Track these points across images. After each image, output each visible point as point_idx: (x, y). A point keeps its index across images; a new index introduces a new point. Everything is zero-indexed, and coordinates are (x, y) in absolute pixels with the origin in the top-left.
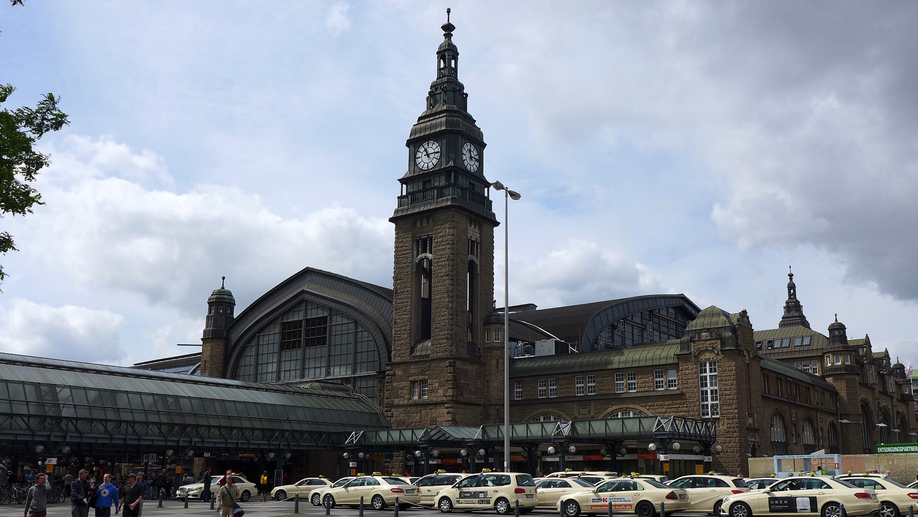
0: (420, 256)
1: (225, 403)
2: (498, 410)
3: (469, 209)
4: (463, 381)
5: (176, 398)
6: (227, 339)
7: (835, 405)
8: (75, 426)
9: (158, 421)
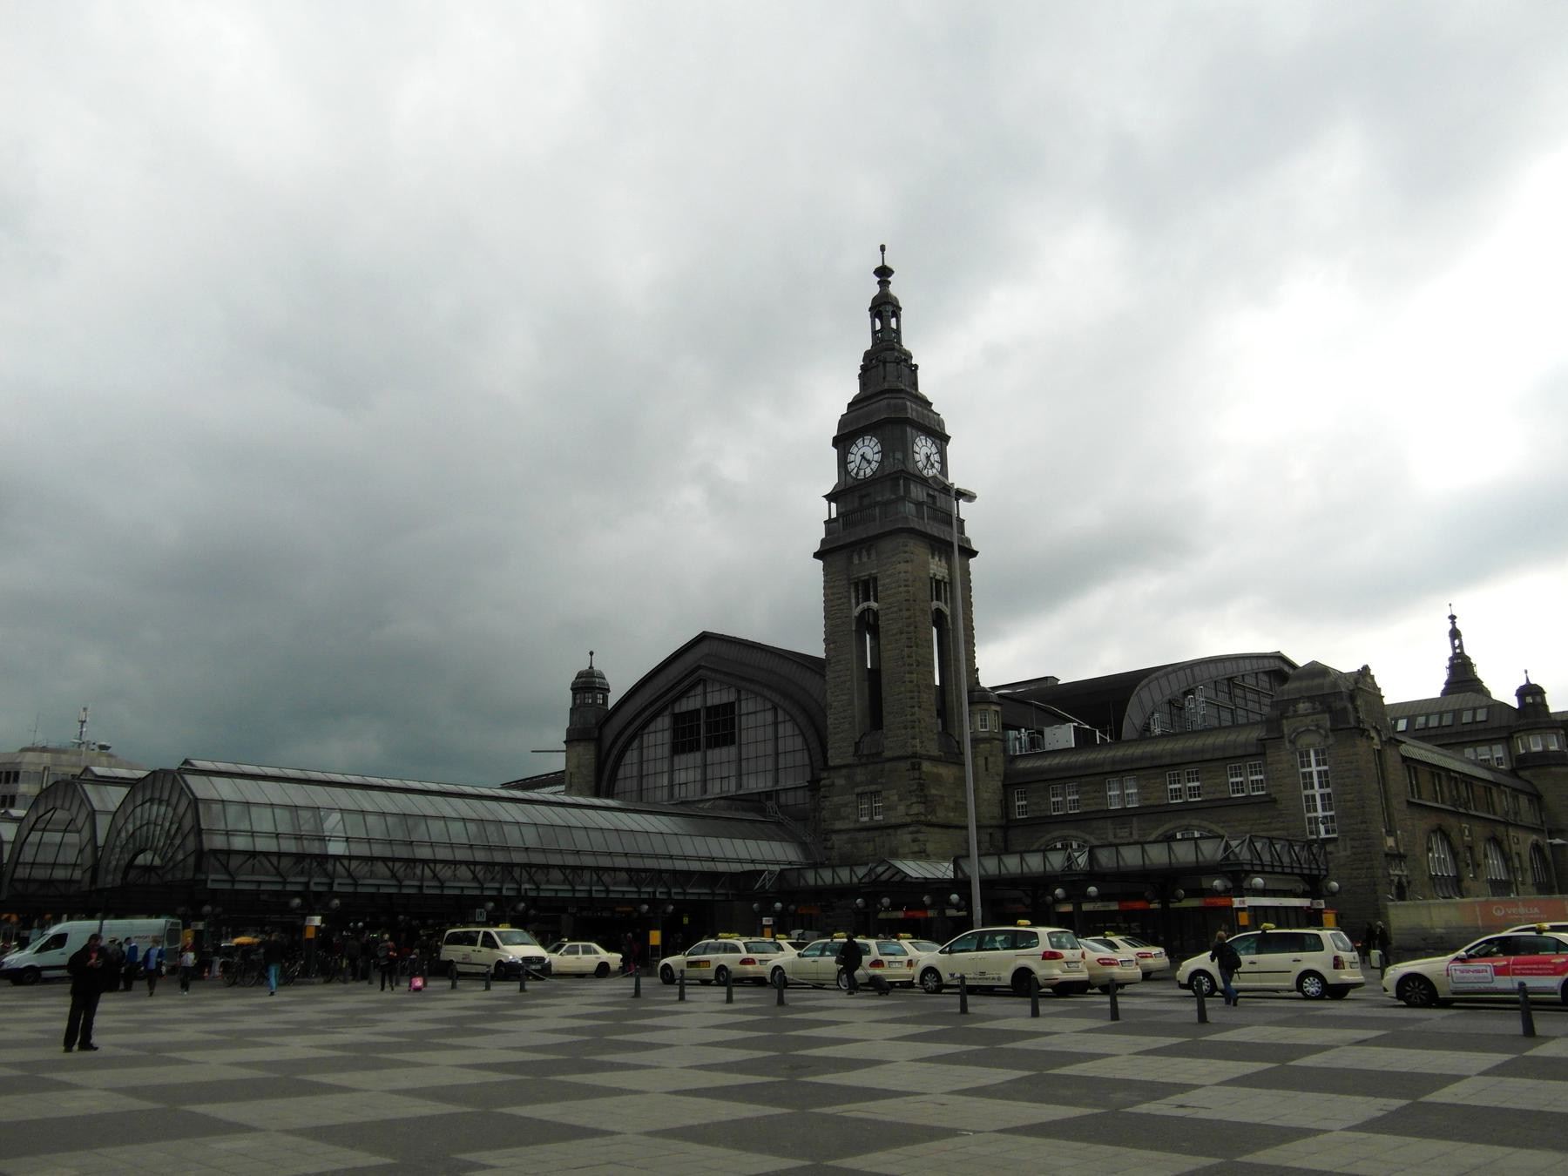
0: (861, 606)
1: (486, 826)
2: (991, 834)
3: (929, 531)
4: (934, 792)
6: (599, 741)
7: (1538, 816)
8: (433, 872)
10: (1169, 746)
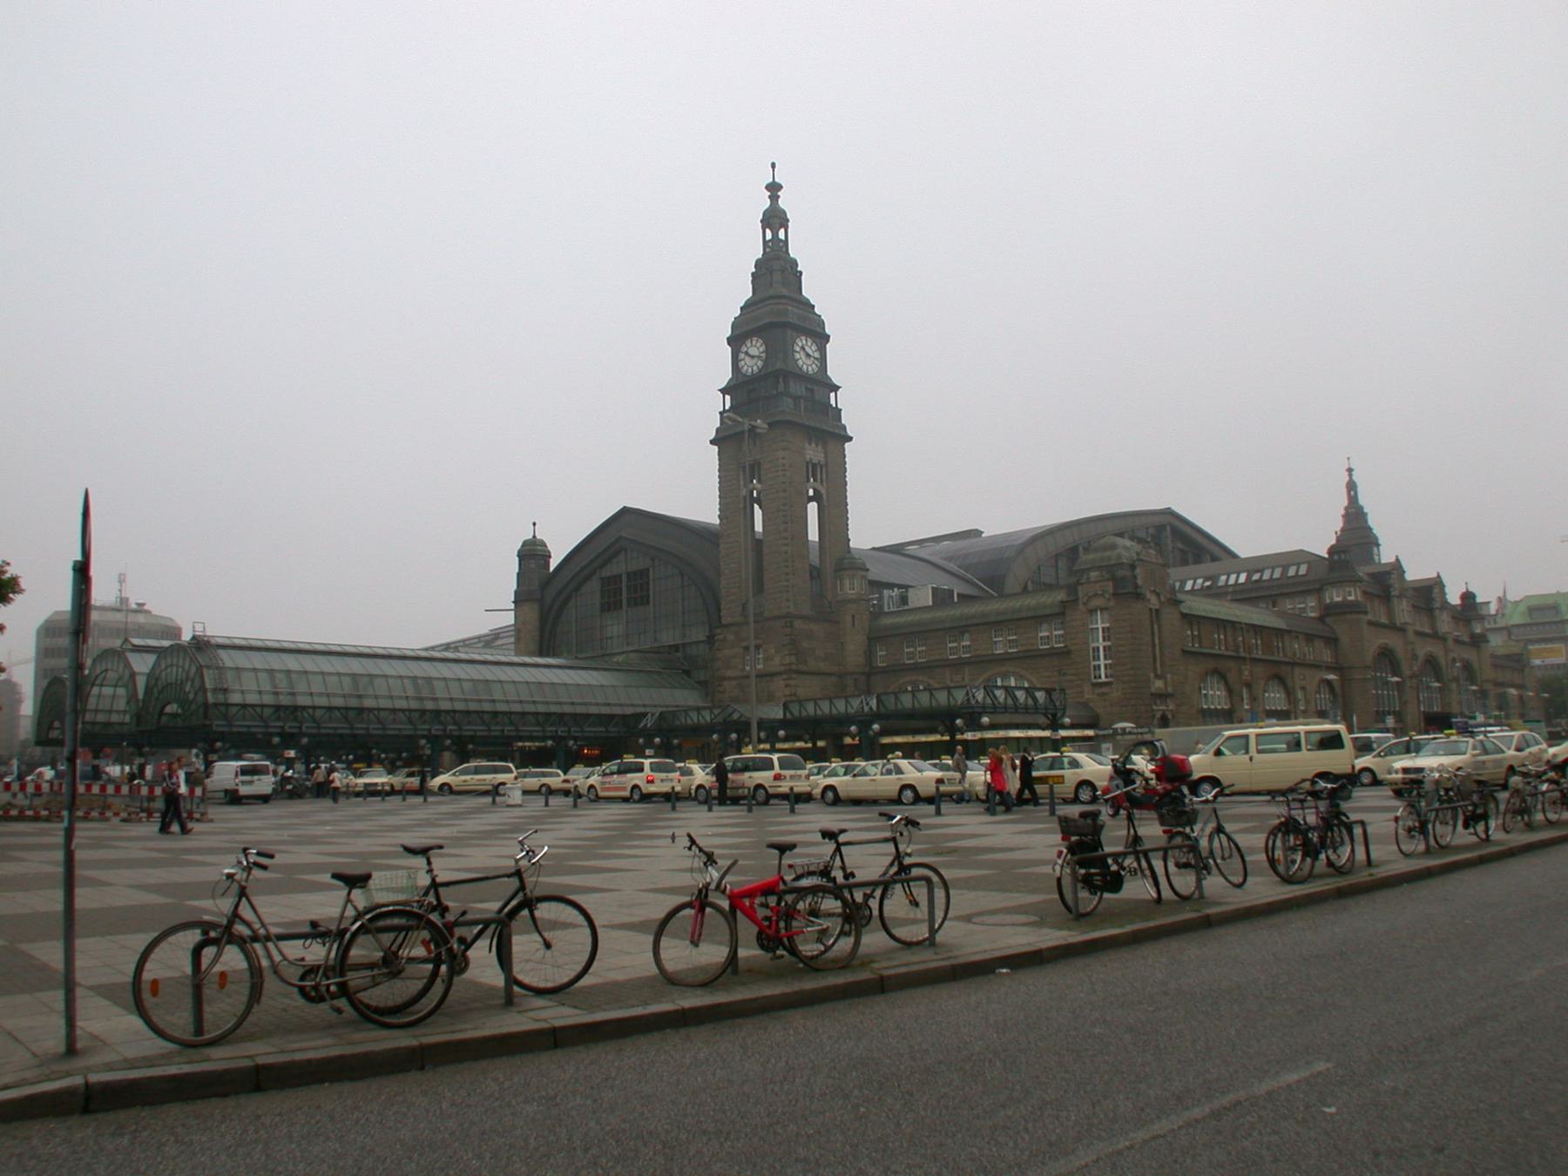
2: (855, 680)
5: (429, 679)
9: (479, 709)
10: (1030, 601)
